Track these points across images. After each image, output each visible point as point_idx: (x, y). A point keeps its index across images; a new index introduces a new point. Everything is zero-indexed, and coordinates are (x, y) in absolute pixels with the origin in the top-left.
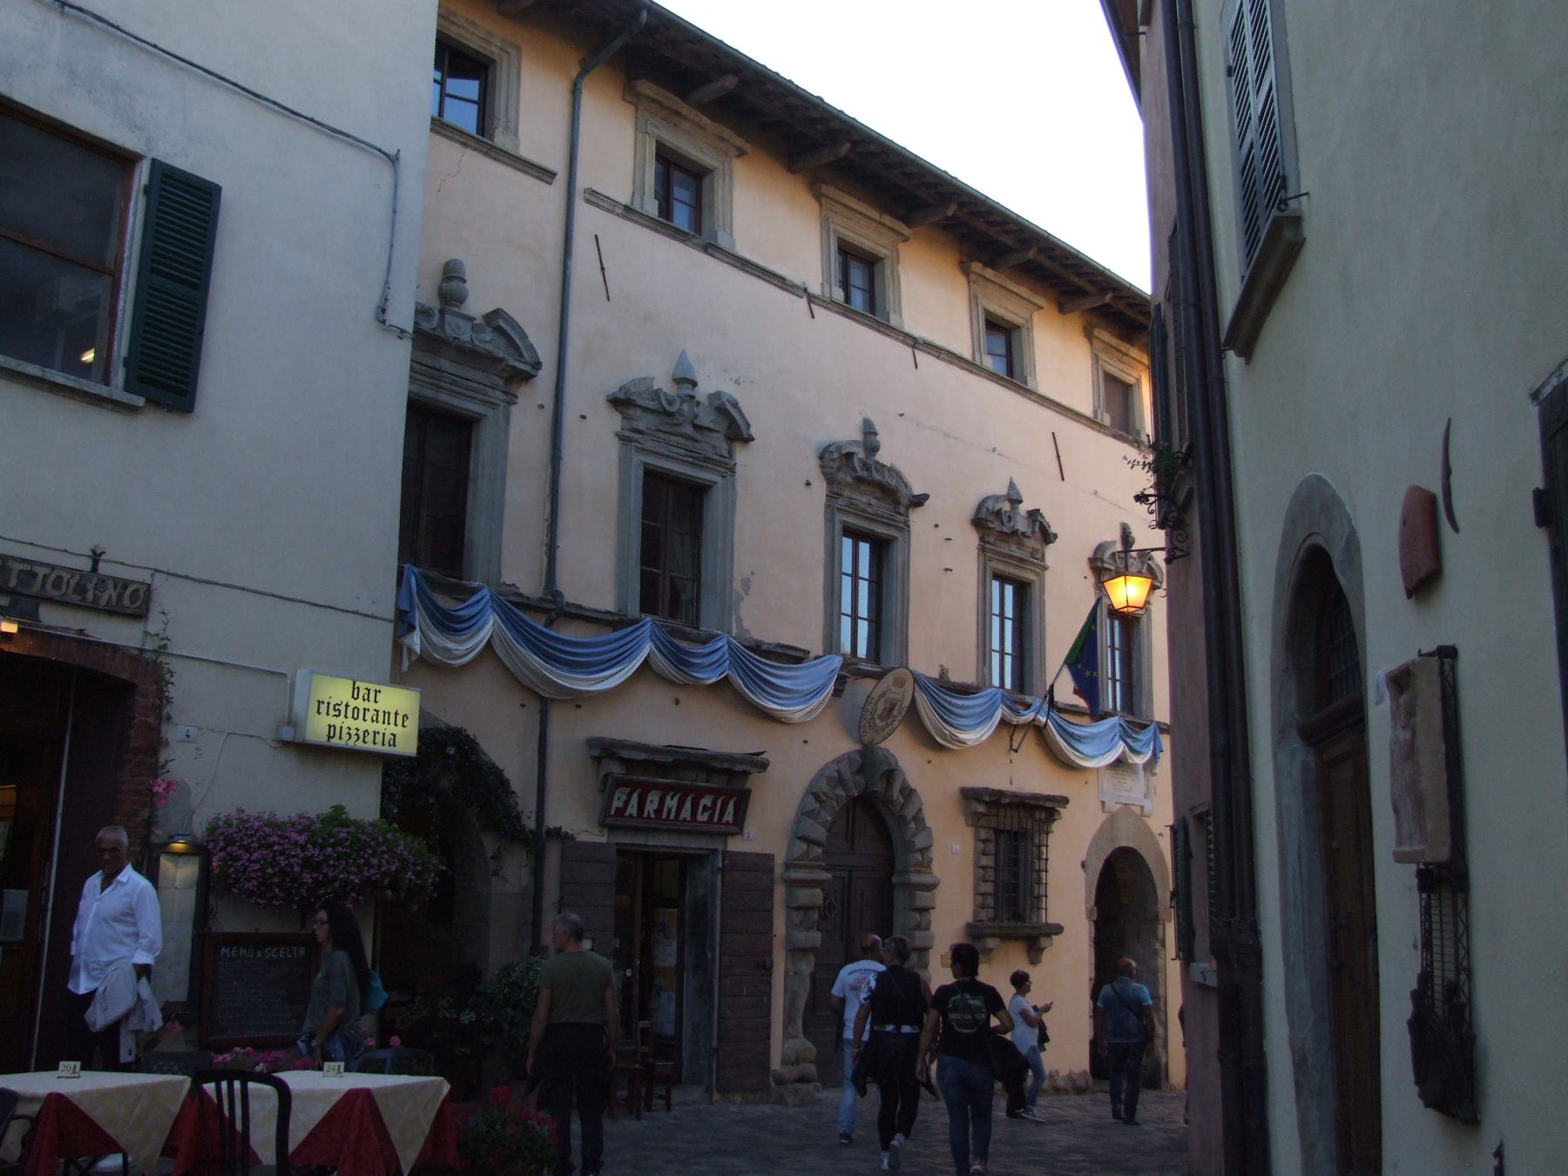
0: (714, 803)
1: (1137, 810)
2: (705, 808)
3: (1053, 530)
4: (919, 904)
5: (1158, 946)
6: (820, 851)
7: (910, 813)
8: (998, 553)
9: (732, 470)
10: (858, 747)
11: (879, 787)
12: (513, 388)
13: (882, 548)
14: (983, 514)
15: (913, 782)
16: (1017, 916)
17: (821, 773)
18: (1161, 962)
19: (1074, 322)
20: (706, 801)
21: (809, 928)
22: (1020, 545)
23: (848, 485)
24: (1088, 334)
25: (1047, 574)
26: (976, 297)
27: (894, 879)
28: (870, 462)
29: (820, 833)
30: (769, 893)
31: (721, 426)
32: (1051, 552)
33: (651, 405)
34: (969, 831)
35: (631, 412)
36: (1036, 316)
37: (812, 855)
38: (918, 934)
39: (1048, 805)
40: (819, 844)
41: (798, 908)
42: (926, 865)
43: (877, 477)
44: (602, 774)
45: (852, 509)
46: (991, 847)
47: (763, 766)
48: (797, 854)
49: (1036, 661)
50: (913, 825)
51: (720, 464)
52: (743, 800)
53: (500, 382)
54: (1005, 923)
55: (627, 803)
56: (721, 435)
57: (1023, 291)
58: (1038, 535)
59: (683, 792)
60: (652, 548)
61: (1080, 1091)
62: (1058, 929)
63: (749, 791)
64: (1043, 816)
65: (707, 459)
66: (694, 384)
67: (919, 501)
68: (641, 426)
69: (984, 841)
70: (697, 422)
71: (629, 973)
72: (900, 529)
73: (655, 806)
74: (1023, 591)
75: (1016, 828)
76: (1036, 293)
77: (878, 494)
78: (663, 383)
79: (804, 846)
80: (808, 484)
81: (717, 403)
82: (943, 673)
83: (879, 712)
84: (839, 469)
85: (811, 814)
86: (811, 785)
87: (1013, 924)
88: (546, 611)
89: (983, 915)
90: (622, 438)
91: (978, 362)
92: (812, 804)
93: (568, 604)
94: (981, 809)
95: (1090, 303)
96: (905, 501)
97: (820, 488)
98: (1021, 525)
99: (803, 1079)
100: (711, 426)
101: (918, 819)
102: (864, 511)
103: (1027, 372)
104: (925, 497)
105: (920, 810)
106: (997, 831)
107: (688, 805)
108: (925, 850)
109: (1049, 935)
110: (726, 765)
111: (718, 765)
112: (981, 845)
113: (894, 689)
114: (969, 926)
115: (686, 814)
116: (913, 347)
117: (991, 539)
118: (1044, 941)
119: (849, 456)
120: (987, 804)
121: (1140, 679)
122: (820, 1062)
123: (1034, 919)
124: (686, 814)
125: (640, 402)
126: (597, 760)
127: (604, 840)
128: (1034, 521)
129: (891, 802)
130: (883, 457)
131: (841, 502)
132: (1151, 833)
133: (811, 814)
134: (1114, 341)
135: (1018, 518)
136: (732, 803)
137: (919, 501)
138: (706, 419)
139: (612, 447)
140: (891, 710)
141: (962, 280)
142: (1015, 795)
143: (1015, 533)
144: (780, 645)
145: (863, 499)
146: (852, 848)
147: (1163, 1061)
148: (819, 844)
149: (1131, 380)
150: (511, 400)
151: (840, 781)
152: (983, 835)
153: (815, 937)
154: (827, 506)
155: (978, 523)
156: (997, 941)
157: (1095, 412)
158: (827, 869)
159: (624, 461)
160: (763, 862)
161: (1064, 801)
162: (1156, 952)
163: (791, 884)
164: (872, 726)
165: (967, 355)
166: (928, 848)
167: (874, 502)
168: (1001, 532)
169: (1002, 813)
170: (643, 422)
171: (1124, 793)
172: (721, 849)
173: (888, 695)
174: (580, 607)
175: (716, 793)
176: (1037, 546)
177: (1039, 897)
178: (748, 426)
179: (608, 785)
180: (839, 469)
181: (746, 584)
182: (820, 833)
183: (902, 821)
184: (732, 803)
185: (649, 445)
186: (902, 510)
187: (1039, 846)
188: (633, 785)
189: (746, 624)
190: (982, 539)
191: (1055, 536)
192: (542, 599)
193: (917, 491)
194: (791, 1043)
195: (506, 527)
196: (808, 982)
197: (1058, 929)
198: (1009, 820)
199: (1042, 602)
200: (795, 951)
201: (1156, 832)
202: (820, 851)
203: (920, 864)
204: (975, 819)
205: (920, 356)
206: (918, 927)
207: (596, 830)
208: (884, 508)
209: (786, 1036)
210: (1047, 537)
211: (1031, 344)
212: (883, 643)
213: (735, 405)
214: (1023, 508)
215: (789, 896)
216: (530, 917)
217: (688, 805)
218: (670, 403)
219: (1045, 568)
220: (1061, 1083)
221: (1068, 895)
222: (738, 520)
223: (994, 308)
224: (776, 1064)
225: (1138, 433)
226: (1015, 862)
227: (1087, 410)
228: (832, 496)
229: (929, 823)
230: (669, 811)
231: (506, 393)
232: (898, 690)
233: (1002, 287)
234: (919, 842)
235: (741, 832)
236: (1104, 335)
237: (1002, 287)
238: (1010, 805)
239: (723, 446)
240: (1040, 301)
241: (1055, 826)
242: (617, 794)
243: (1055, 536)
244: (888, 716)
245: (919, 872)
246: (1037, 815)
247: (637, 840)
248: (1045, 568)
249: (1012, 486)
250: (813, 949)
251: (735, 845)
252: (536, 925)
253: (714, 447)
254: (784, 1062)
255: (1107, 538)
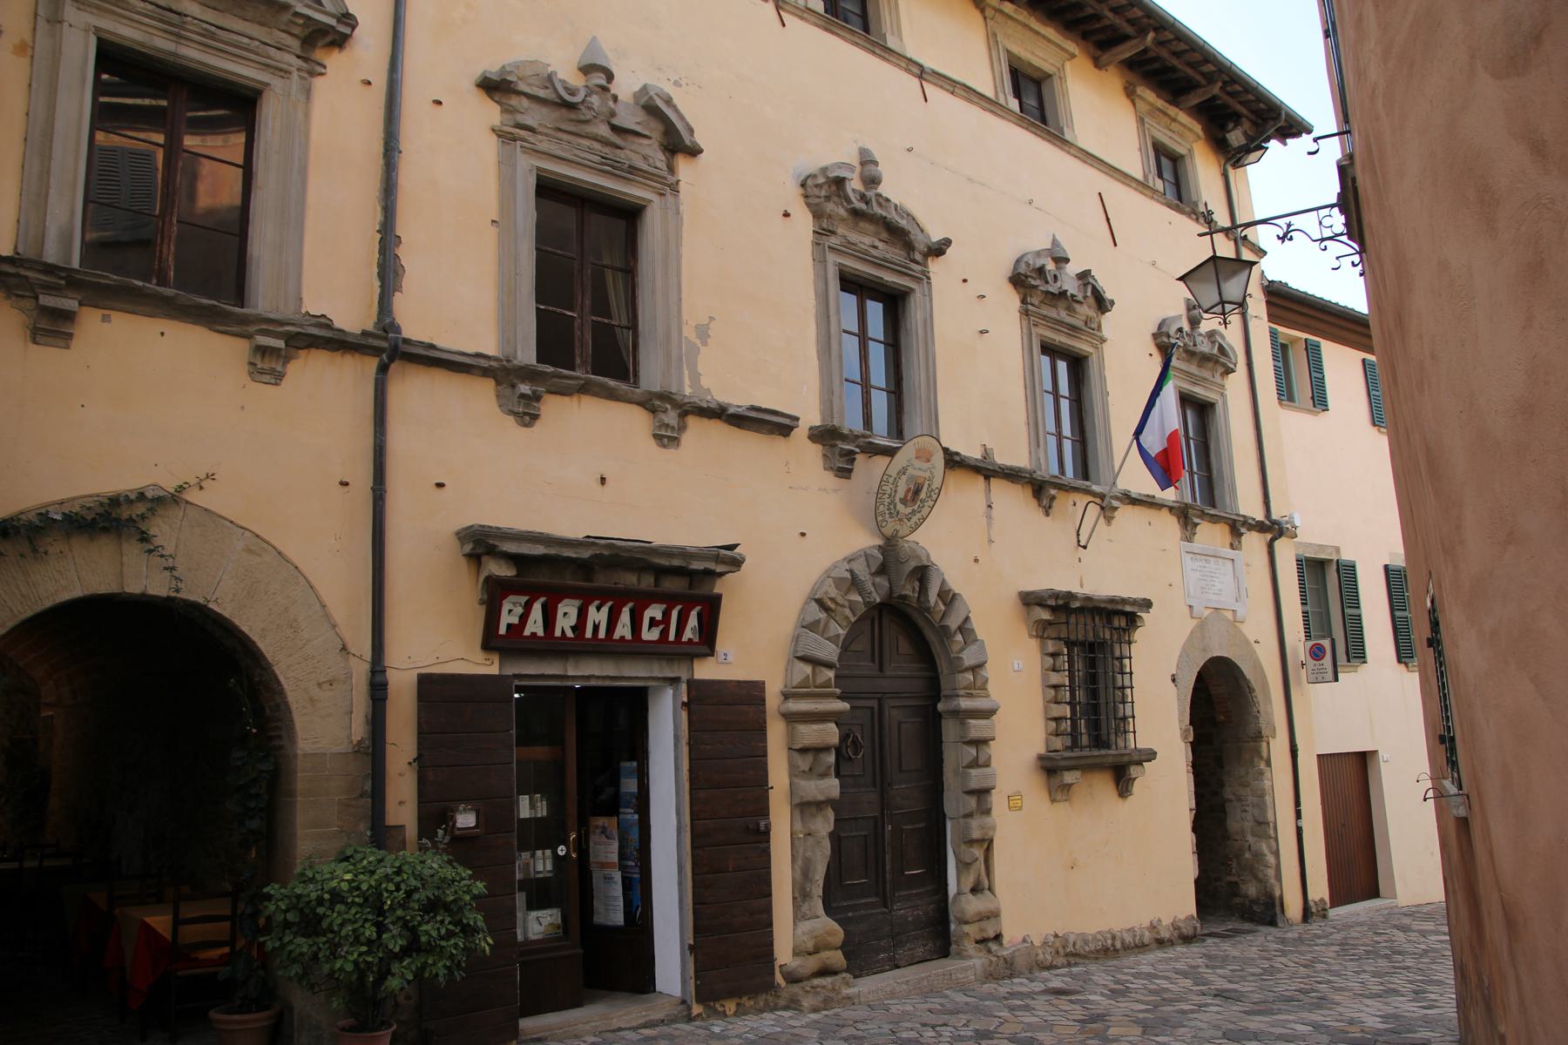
0: (667, 614)
1: (1229, 615)
2: (653, 623)
3: (1108, 295)
4: (974, 734)
5: (1263, 766)
6: (831, 674)
7: (953, 622)
8: (1045, 317)
9: (674, 188)
10: (880, 542)
11: (909, 590)
12: (318, 54)
13: (895, 302)
14: (1022, 269)
15: (955, 585)
16: (1099, 742)
17: (827, 574)
18: (1267, 783)
19: (1113, 80)
20: (655, 611)
21: (824, 775)
22: (1070, 309)
23: (843, 220)
24: (1130, 93)
25: (1106, 346)
26: (995, 35)
27: (940, 707)
28: (871, 194)
29: (830, 652)
30: (761, 729)
31: (654, 130)
32: (1109, 322)
33: (542, 93)
34: (1034, 644)
35: (514, 101)
36: (1068, 66)
37: (820, 680)
38: (973, 772)
39: (1128, 609)
40: (829, 666)
41: (804, 751)
42: (980, 687)
43: (879, 211)
44: (482, 579)
45: (848, 249)
46: (1063, 661)
47: (737, 563)
48: (797, 679)
49: (1101, 445)
50: (959, 637)
51: (660, 179)
52: (711, 611)
53: (295, 44)
54: (1086, 752)
55: (524, 618)
56: (656, 145)
57: (1049, 32)
58: (1091, 301)
59: (616, 599)
60: (553, 281)
61: (1187, 939)
62: (1151, 755)
63: (719, 598)
64: (1123, 624)
65: (633, 169)
66: (610, 77)
67: (939, 250)
68: (529, 121)
69: (1054, 655)
70: (615, 121)
71: (562, 850)
72: (918, 280)
73: (573, 620)
74: (1078, 364)
75: (1091, 638)
76: (1067, 38)
77: (884, 235)
78: (567, 72)
79: (808, 669)
80: (786, 215)
81: (642, 102)
82: (987, 453)
83: (900, 494)
84: (828, 198)
85: (812, 626)
86: (814, 590)
87: (1096, 753)
88: (376, 351)
89: (1058, 743)
90: (499, 133)
91: (1002, 101)
92: (817, 613)
93: (407, 341)
94: (1045, 615)
95: (1127, 51)
96: (921, 246)
97: (804, 223)
98: (1071, 287)
99: (824, 972)
100: (638, 129)
101: (965, 628)
102: (866, 253)
103: (1063, 122)
104: (947, 242)
105: (967, 619)
106: (1070, 644)
107: (625, 617)
108: (976, 668)
109: (1140, 763)
110: (676, 562)
111: (664, 562)
112: (1050, 660)
113: (918, 464)
114: (1041, 758)
115: (623, 629)
116: (920, 77)
117: (1036, 301)
118: (1134, 771)
119: (840, 182)
120: (1054, 609)
121: (1220, 471)
122: (847, 948)
123: (1121, 743)
124: (623, 629)
125: (522, 87)
126: (475, 558)
127: (493, 670)
128: (1085, 285)
129: (928, 609)
130: (884, 189)
131: (833, 241)
132: (1247, 641)
133: (812, 626)
134: (1160, 103)
135: (1065, 278)
136: (694, 615)
137: (939, 250)
138: (629, 118)
139: (489, 147)
140: (917, 492)
141: (977, 15)
142: (1088, 599)
143: (1063, 294)
144: (753, 408)
145: (865, 239)
146: (881, 670)
147: (1277, 894)
148: (829, 666)
149: (1181, 150)
150: (314, 70)
151: (854, 583)
152: (1051, 646)
153: (832, 786)
154: (816, 244)
155: (1017, 281)
156: (1077, 774)
157: (1145, 176)
158: (842, 698)
159: (506, 165)
160: (752, 693)
161: (1147, 604)
162: (1261, 773)
163: (791, 718)
164: (894, 514)
165: (990, 93)
166: (981, 666)
167: (880, 245)
168: (1047, 293)
169: (1073, 620)
170: (535, 116)
171: (1212, 597)
172: (684, 677)
173: (910, 471)
174: (432, 347)
175: (669, 600)
176: (1092, 313)
177: (1124, 719)
178: (691, 131)
179: (495, 593)
180: (828, 198)
181: (703, 332)
182: (830, 652)
183: (944, 632)
184: (694, 615)
185: (544, 145)
186: (918, 257)
187: (1121, 658)
188: (532, 593)
189: (705, 382)
190: (1024, 301)
191: (1112, 303)
192: (365, 333)
193: (936, 236)
194: (806, 926)
195: (308, 238)
196: (827, 844)
197: (1151, 755)
198: (1082, 630)
199: (1103, 379)
200: (805, 808)
201: (1252, 639)
202: (831, 674)
203: (973, 686)
204: (1042, 631)
205: (929, 88)
206: (975, 764)
207: (479, 656)
208: (895, 254)
209: (799, 916)
210: (1102, 304)
211: (1065, 94)
212: (906, 418)
213: (669, 101)
214: (1073, 269)
215: (791, 736)
216: (368, 786)
217: (625, 617)
218: (572, 93)
219: (1103, 341)
220: (1165, 934)
221: (1158, 715)
222: (685, 250)
223: (1017, 50)
224: (784, 953)
225: (1196, 204)
226: (1092, 678)
227: (1139, 175)
228: (822, 233)
229: (980, 635)
230: (596, 628)
231: (305, 59)
232: (925, 466)
233: (1026, 26)
234: (968, 657)
235: (711, 651)
236: (1148, 95)
237: (1026, 26)
238: (1081, 610)
239: (659, 158)
240: (1071, 46)
241: (1138, 635)
242: (506, 606)
243: (1112, 303)
244: (914, 500)
245: (971, 696)
246: (1116, 624)
247: (551, 668)
248: (1103, 341)
249: (1055, 242)
250: (830, 802)
251: (705, 670)
252: (377, 794)
253: (645, 158)
254: (797, 953)
255: (1171, 313)
